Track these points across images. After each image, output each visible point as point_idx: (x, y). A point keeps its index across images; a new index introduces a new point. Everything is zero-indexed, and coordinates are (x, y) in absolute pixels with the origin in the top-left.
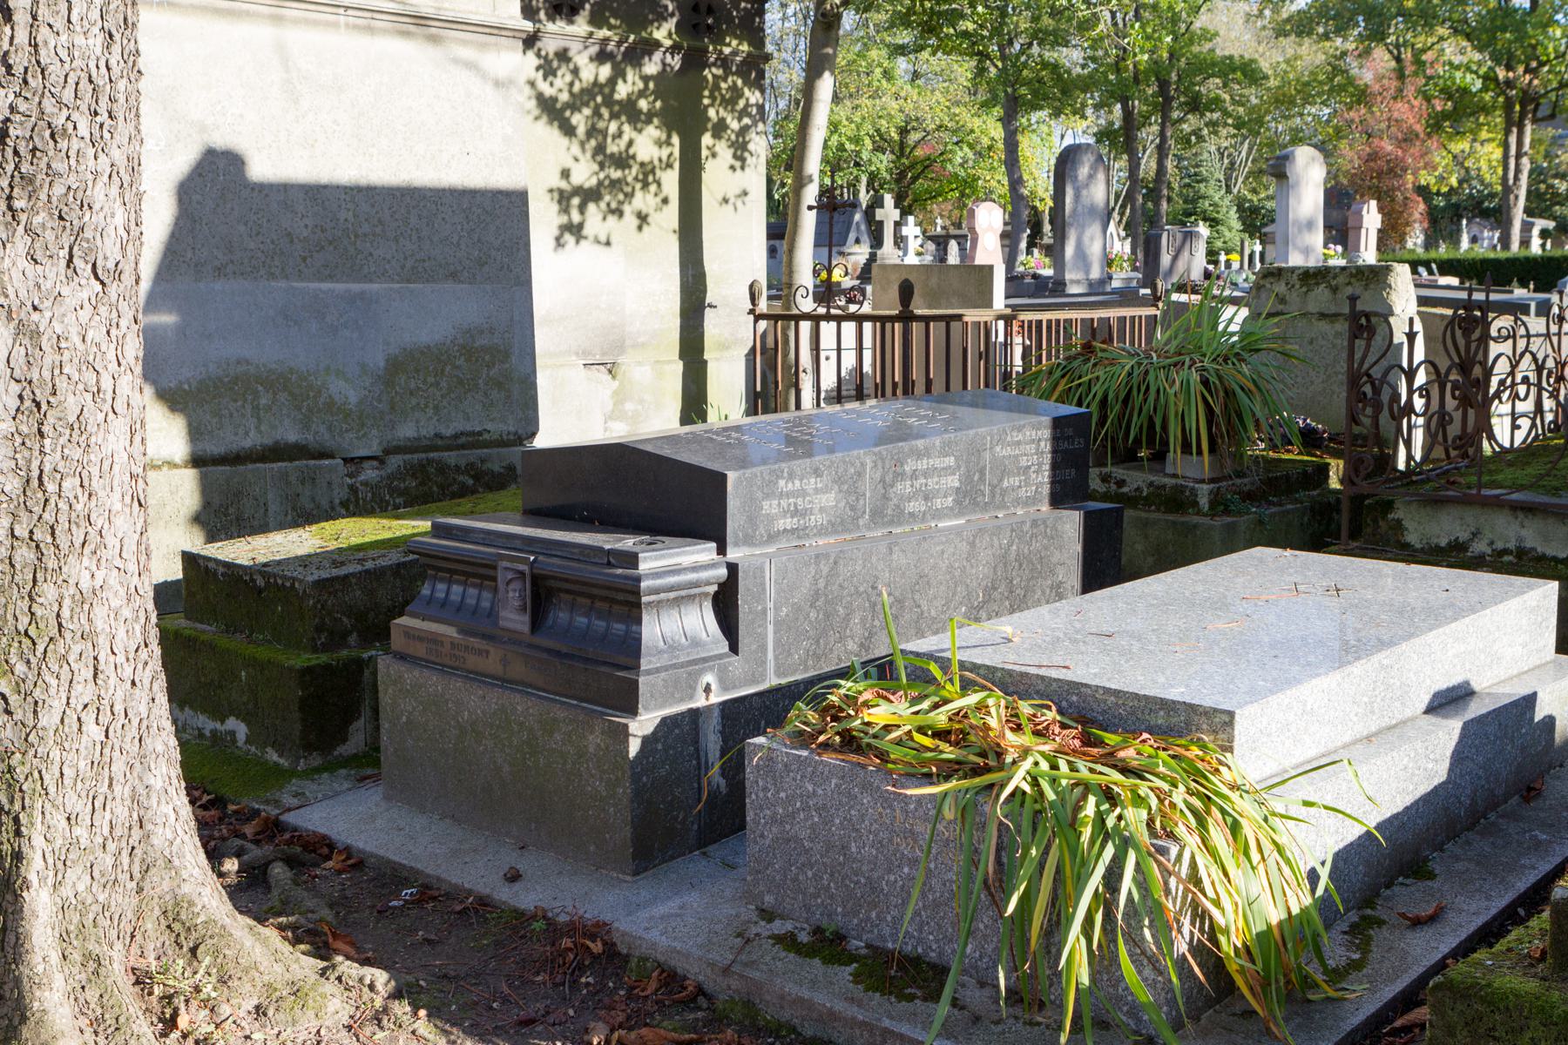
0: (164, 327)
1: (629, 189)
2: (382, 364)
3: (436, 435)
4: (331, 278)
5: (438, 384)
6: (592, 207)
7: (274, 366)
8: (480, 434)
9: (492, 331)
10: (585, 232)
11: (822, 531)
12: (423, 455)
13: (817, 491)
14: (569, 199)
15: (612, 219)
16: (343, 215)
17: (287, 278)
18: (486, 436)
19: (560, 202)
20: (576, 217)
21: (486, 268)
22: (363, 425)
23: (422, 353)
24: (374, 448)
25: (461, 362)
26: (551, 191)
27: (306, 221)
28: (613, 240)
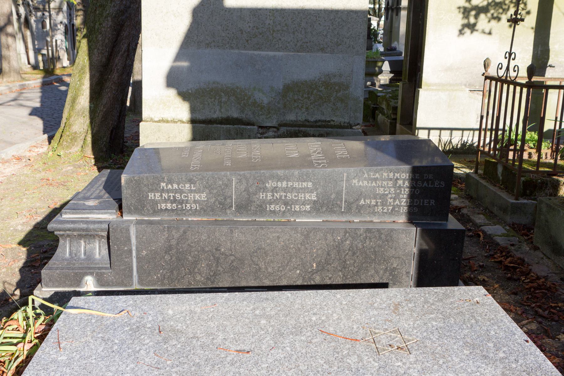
0: (183, 67)
1: (506, 7)
2: (281, 87)
3: (306, 120)
4: (259, 49)
5: (309, 98)
6: (482, 16)
7: (230, 85)
8: (329, 121)
9: (340, 76)
10: (477, 28)
11: (195, 213)
12: (297, 129)
13: (191, 191)
14: (469, 12)
15: (493, 22)
16: (268, 22)
17: (238, 48)
18: (332, 123)
19: (464, 13)
20: (472, 20)
21: (341, 47)
22: (269, 113)
23: (302, 84)
24: (274, 123)
25: (322, 89)
26: (459, 8)
27: (250, 24)
28: (493, 32)
